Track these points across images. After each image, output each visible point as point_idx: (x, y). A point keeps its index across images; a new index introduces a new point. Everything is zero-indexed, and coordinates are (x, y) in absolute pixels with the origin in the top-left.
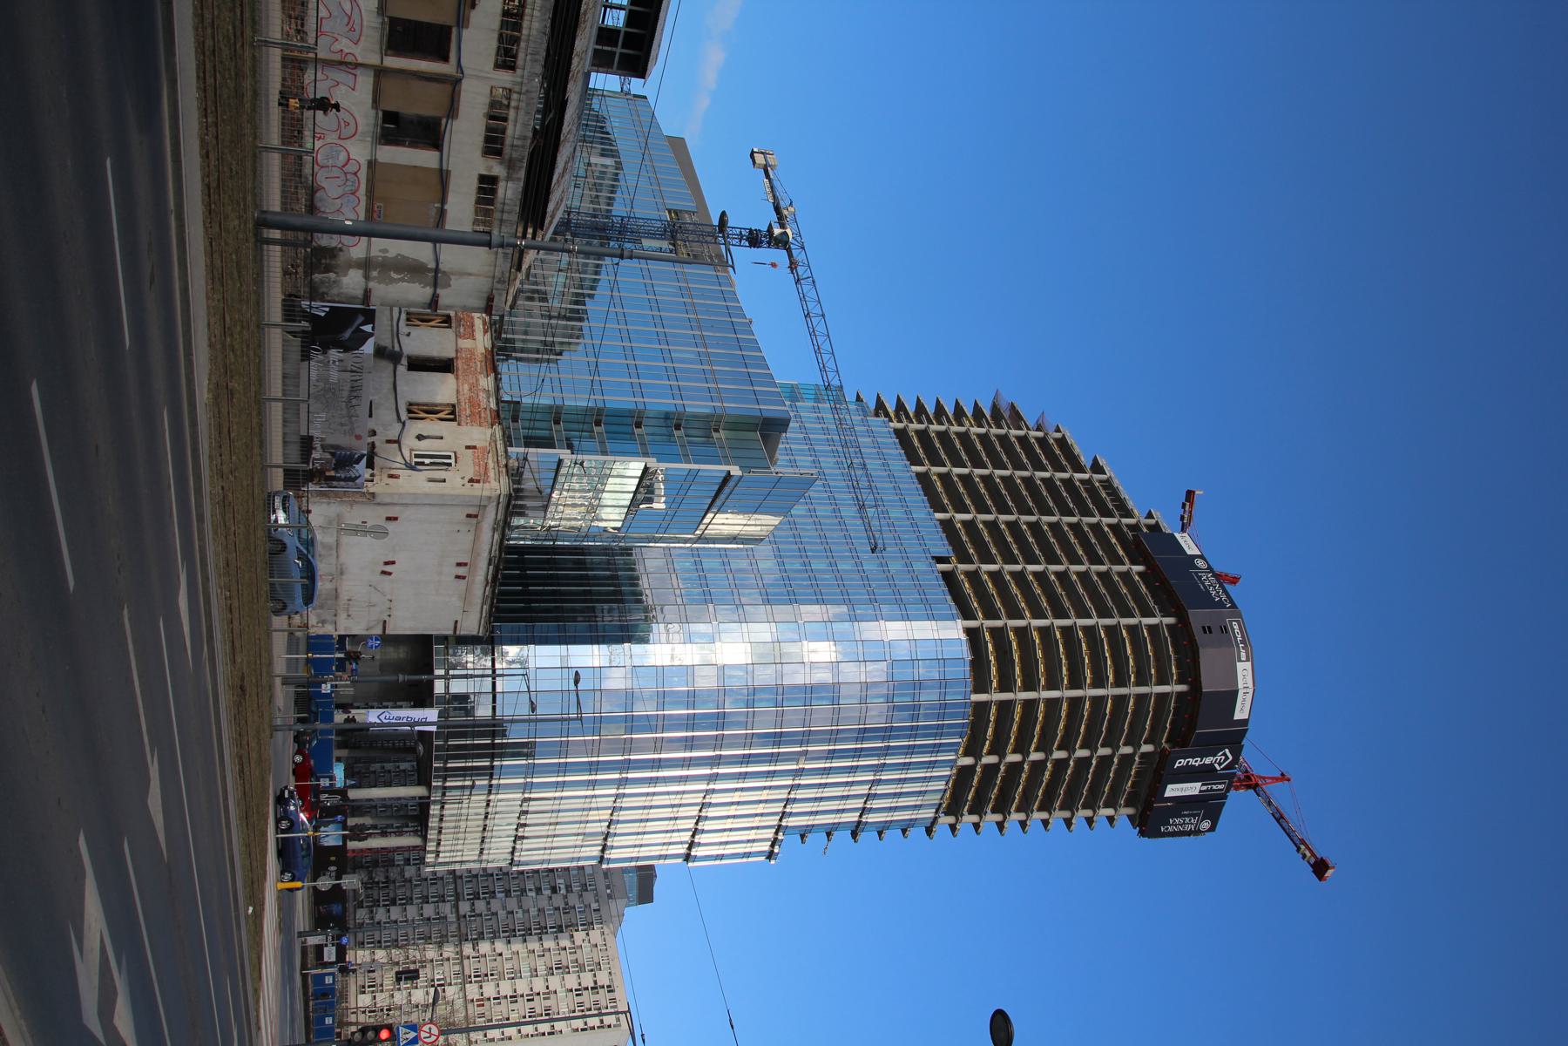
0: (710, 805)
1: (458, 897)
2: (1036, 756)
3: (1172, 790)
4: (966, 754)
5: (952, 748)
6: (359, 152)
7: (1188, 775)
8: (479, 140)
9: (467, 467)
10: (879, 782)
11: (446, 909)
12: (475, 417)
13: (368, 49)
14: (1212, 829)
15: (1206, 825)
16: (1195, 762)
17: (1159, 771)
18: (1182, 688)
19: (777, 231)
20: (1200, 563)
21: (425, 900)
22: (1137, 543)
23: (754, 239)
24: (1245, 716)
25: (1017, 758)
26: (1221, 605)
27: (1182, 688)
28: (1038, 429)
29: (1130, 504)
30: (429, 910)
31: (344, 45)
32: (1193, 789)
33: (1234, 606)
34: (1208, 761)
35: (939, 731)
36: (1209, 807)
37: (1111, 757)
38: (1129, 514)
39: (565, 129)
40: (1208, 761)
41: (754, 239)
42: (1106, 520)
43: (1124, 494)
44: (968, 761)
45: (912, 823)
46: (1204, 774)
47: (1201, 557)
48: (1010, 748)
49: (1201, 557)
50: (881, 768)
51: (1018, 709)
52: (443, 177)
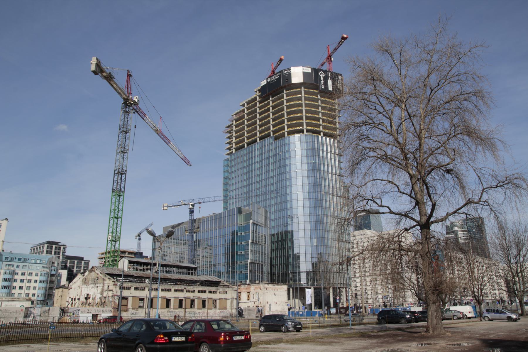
0: (335, 152)
1: (365, 276)
2: (321, 128)
3: (330, 88)
4: (320, 134)
5: (318, 137)
6: (218, 311)
7: (326, 84)
8: (204, 294)
9: (258, 290)
10: (327, 150)
11: (368, 279)
12: (249, 289)
13: (205, 310)
14: (341, 75)
15: (340, 77)
16: (322, 82)
17: (325, 92)
18: (303, 88)
19: (191, 207)
20: (269, 80)
21: (366, 284)
22: (264, 97)
23: (192, 212)
24: (310, 69)
25: (320, 114)
26: (280, 76)
27: (303, 88)
28: (233, 121)
29: (253, 97)
30: (368, 284)
31: (206, 314)
32: (330, 82)
33: (280, 72)
34: (322, 79)
35: (313, 142)
36: (335, 77)
37: (324, 133)
38: (256, 98)
39: (211, 280)
40: (322, 79)
41: (192, 212)
42: (258, 105)
43: (250, 99)
44: (322, 134)
45: (339, 161)
46: (326, 79)
47: (267, 79)
48: (318, 123)
49: (267, 79)
50: (323, 150)
51: (307, 115)
52: (220, 299)
